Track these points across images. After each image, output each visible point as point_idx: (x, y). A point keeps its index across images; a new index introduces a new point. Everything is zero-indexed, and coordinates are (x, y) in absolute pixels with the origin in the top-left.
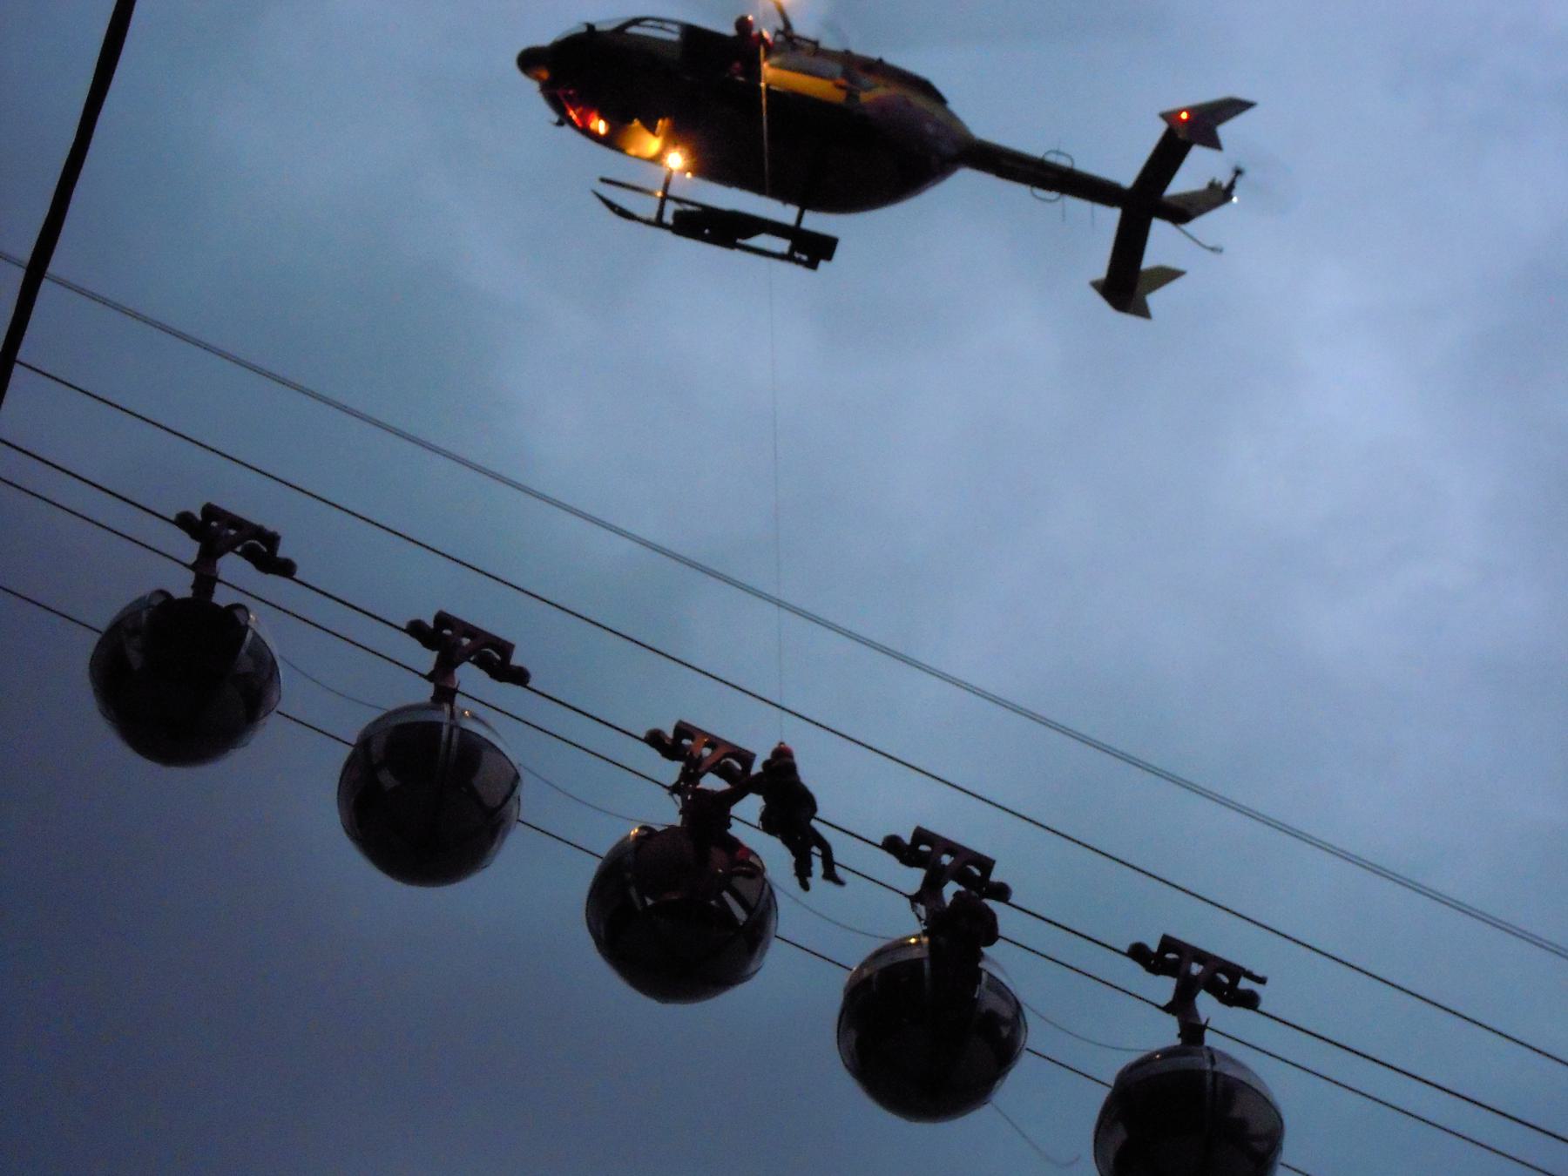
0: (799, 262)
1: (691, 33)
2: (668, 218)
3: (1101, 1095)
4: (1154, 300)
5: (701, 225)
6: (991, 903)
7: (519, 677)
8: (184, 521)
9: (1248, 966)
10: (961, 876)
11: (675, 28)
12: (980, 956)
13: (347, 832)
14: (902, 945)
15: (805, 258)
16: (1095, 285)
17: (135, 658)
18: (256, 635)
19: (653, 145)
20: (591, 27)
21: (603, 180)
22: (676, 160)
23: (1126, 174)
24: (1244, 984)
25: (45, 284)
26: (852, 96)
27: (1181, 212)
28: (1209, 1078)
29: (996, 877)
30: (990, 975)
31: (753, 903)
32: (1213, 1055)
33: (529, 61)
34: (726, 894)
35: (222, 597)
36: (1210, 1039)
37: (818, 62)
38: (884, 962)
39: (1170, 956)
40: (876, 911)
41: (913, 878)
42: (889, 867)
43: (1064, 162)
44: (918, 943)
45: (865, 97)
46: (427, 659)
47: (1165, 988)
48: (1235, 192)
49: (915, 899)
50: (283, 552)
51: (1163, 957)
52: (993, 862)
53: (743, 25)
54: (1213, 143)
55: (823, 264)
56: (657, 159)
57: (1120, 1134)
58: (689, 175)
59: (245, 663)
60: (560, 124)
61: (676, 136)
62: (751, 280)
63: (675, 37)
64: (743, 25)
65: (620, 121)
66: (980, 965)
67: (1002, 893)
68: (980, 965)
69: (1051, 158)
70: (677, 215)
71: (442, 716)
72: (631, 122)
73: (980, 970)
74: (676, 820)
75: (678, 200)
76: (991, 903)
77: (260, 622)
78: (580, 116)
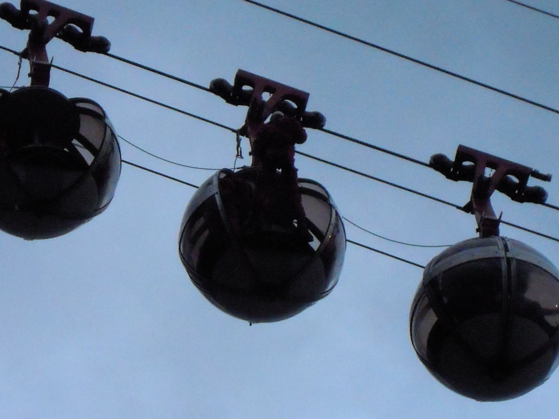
24: (532, 182)
28: (504, 264)
29: (310, 108)
31: (98, 147)
34: (75, 142)
36: (504, 231)
39: (466, 163)
40: (219, 147)
41: (238, 115)
42: (437, 182)
46: (21, 38)
47: (464, 191)
51: (460, 165)
52: (308, 95)
57: (431, 319)
74: (248, 161)
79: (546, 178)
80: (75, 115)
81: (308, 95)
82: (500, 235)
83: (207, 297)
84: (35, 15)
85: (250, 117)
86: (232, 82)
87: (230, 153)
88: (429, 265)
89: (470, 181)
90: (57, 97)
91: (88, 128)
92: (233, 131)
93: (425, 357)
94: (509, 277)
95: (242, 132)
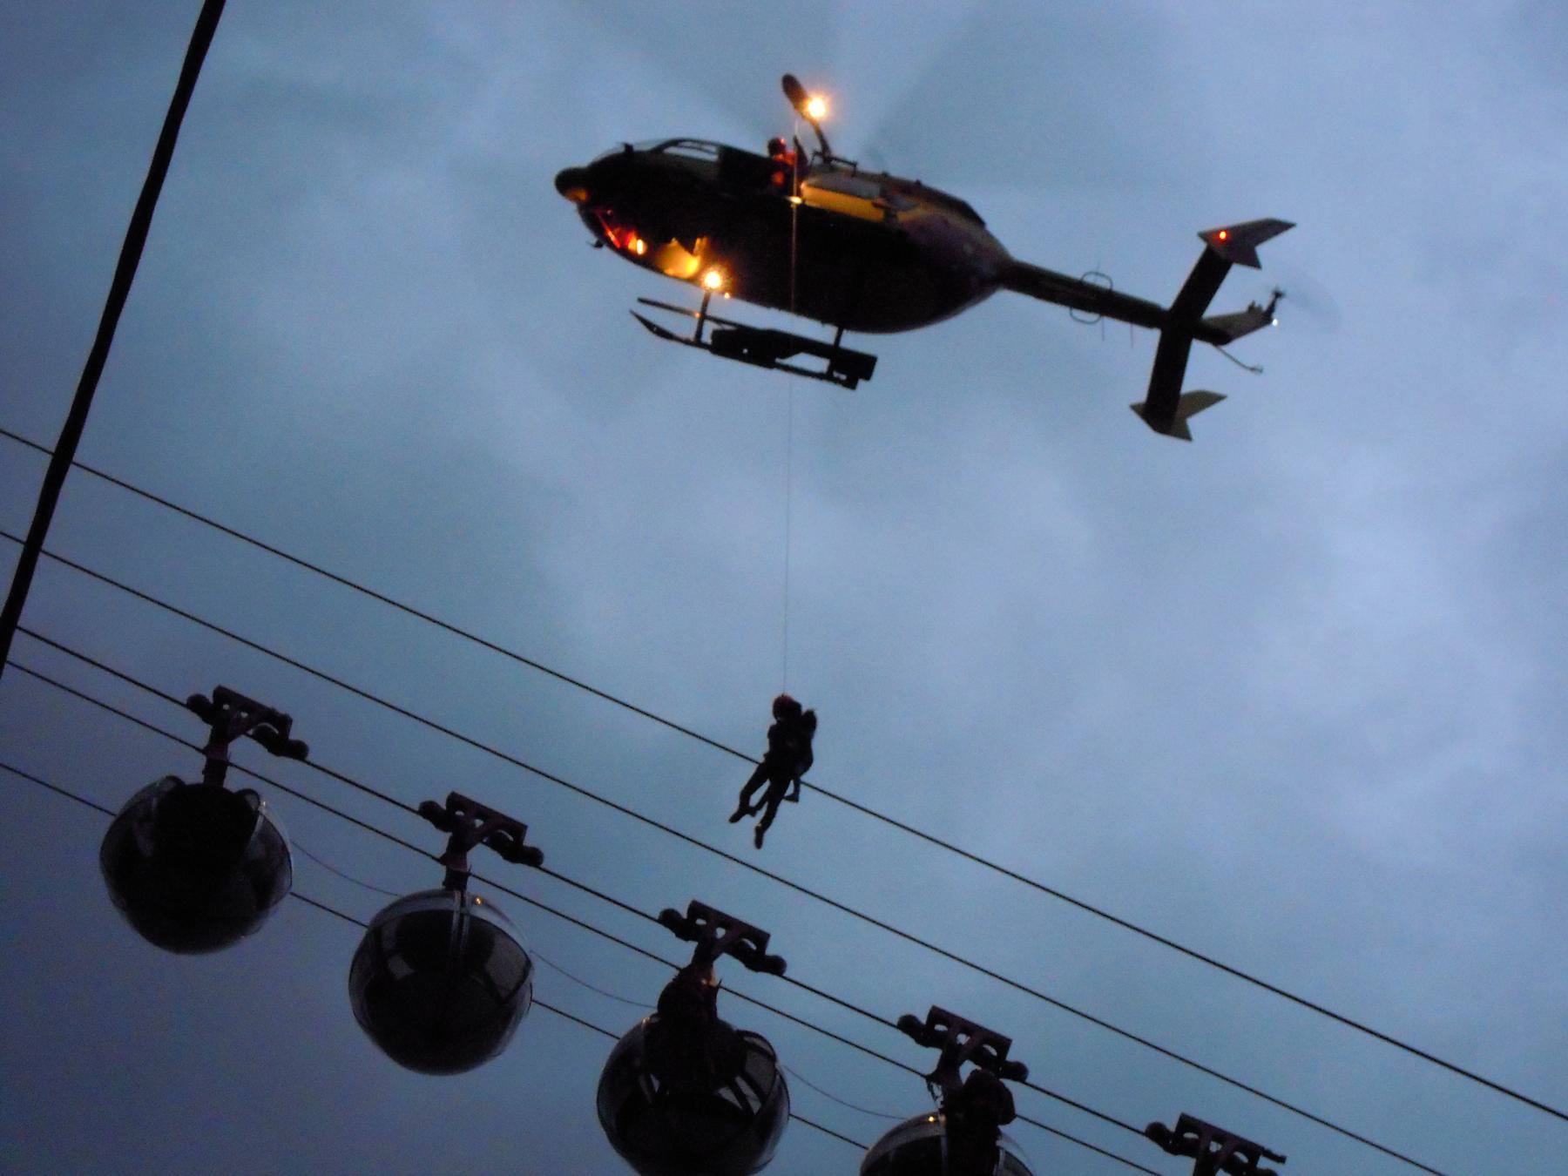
0: (837, 381)
1: (730, 155)
2: (707, 338)
4: (1195, 423)
5: (736, 343)
6: (1010, 1084)
7: (533, 858)
8: (196, 704)
9: (1267, 1145)
10: (977, 1055)
11: (713, 149)
12: (998, 1134)
13: (360, 1022)
14: (921, 1122)
15: (843, 377)
16: (1135, 408)
17: (147, 847)
18: (266, 820)
20: (628, 148)
21: (642, 301)
22: (714, 279)
23: (1165, 296)
25: (42, 558)
26: (889, 215)
27: (1221, 334)
29: (1012, 1056)
30: (1008, 1154)
33: (567, 182)
35: (234, 782)
36: (473, 886)
37: (856, 184)
38: (901, 1140)
41: (930, 1058)
42: (906, 1047)
43: (1103, 283)
44: (937, 1121)
45: (903, 217)
46: (439, 841)
48: (1275, 315)
49: (931, 1079)
50: (295, 734)
52: (768, 936)
54: (1253, 262)
55: (862, 383)
58: (727, 296)
59: (256, 849)
60: (599, 245)
61: (709, 259)
62: (792, 393)
63: (714, 158)
66: (999, 1143)
67: (1019, 1073)
68: (999, 1143)
69: (1090, 279)
70: (716, 335)
71: (453, 904)
72: (669, 241)
73: (998, 1149)
76: (1010, 1084)
77: (273, 810)
78: (618, 236)
79: (1281, 1160)
81: (768, 936)
84: (943, 1033)
85: (943, 1062)
87: (918, 1102)
91: (754, 1065)
94: (460, 934)
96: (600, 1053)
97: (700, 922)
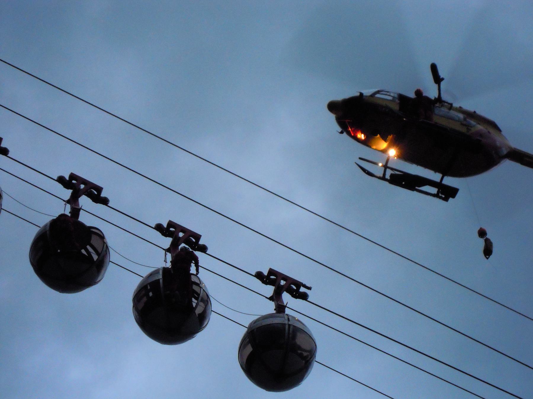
0: (441, 198)
1: (402, 98)
2: (388, 176)
3: (243, 331)
10: (187, 241)
15: (443, 196)
19: (383, 145)
21: (360, 158)
24: (302, 290)
28: (287, 327)
29: (201, 242)
31: (100, 251)
32: (289, 318)
33: (333, 107)
36: (287, 311)
39: (272, 277)
40: (156, 257)
41: (167, 242)
42: (257, 284)
47: (270, 290)
51: (269, 278)
53: (418, 93)
55: (451, 199)
56: (384, 151)
57: (249, 349)
61: (394, 143)
64: (418, 93)
65: (371, 135)
67: (203, 249)
70: (392, 176)
72: (376, 135)
75: (392, 169)
79: (310, 288)
80: (90, 234)
82: (286, 313)
83: (250, 379)
86: (67, 178)
88: (251, 324)
89: (273, 286)
90: (82, 225)
91: (95, 241)
92: (164, 249)
93: (244, 366)
94: (289, 333)
95: (168, 250)
96: (32, 233)
97: (74, 182)
